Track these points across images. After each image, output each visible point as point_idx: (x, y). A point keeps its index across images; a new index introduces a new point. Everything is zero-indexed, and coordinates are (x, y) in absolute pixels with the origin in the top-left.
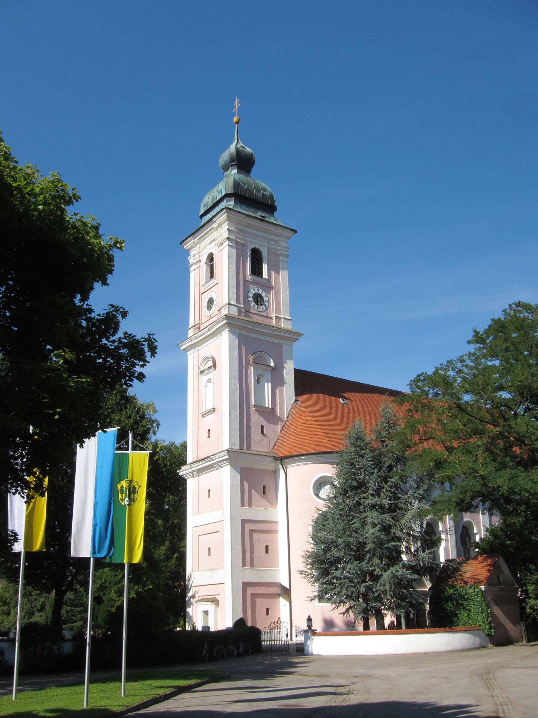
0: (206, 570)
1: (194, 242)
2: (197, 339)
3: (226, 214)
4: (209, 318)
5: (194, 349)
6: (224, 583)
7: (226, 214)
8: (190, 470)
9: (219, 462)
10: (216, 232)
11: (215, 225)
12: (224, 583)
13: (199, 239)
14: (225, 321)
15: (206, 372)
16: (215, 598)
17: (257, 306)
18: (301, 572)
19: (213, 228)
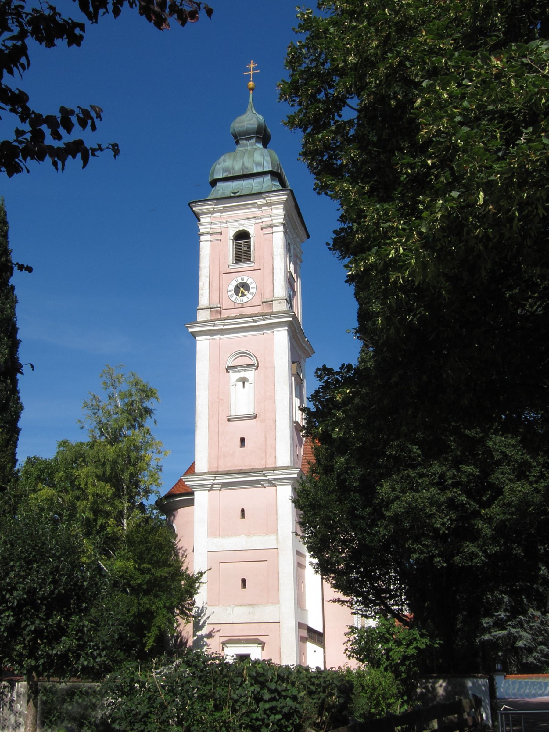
0: (236, 606)
1: (214, 208)
2: (224, 325)
3: (286, 197)
4: (240, 306)
5: (211, 336)
6: (279, 622)
7: (286, 197)
8: (212, 481)
9: (275, 479)
10: (257, 209)
11: (260, 202)
12: (279, 622)
13: (224, 207)
14: (291, 319)
15: (239, 369)
16: (257, 639)
17: (235, 296)
18: (214, 629)
19: (256, 203)
